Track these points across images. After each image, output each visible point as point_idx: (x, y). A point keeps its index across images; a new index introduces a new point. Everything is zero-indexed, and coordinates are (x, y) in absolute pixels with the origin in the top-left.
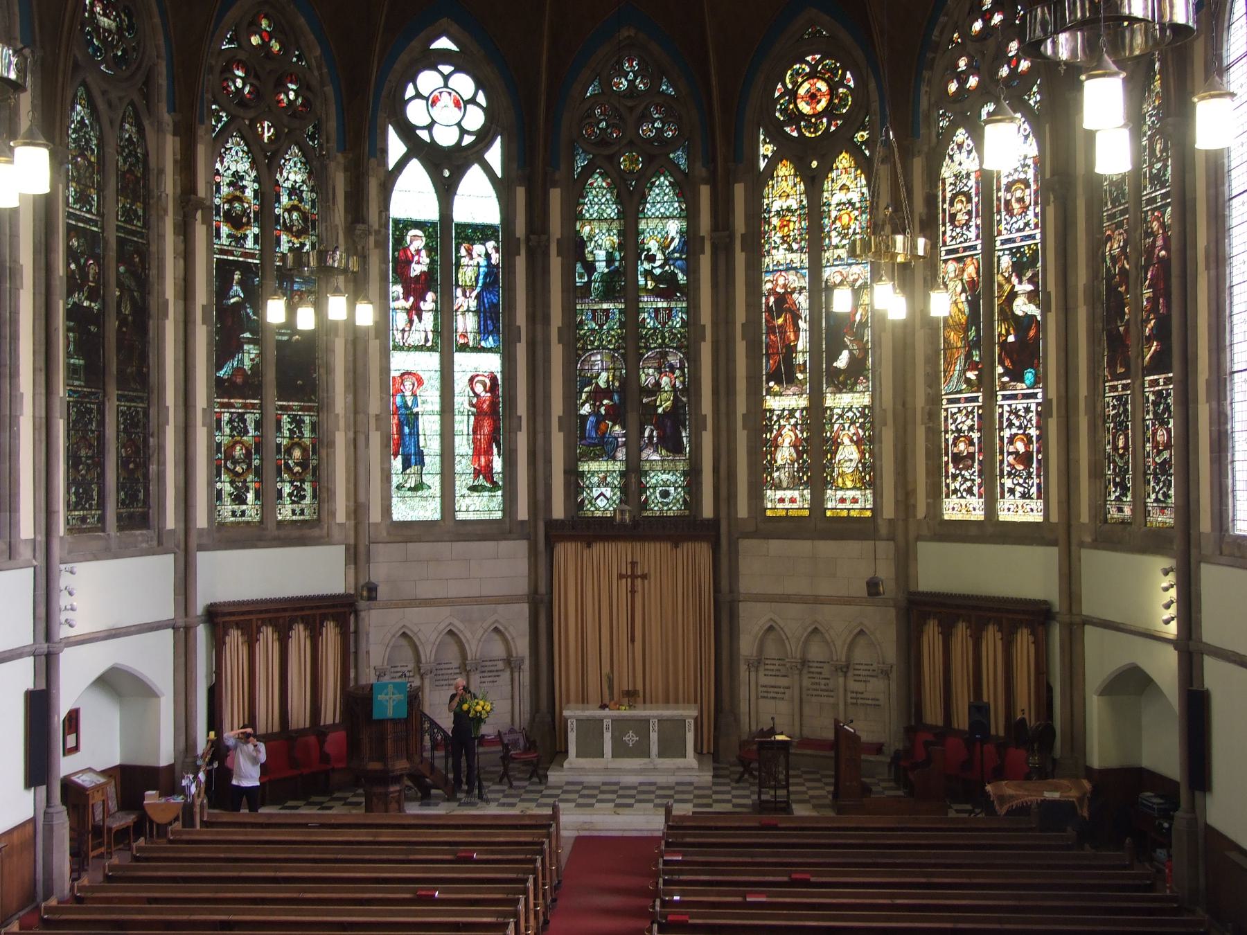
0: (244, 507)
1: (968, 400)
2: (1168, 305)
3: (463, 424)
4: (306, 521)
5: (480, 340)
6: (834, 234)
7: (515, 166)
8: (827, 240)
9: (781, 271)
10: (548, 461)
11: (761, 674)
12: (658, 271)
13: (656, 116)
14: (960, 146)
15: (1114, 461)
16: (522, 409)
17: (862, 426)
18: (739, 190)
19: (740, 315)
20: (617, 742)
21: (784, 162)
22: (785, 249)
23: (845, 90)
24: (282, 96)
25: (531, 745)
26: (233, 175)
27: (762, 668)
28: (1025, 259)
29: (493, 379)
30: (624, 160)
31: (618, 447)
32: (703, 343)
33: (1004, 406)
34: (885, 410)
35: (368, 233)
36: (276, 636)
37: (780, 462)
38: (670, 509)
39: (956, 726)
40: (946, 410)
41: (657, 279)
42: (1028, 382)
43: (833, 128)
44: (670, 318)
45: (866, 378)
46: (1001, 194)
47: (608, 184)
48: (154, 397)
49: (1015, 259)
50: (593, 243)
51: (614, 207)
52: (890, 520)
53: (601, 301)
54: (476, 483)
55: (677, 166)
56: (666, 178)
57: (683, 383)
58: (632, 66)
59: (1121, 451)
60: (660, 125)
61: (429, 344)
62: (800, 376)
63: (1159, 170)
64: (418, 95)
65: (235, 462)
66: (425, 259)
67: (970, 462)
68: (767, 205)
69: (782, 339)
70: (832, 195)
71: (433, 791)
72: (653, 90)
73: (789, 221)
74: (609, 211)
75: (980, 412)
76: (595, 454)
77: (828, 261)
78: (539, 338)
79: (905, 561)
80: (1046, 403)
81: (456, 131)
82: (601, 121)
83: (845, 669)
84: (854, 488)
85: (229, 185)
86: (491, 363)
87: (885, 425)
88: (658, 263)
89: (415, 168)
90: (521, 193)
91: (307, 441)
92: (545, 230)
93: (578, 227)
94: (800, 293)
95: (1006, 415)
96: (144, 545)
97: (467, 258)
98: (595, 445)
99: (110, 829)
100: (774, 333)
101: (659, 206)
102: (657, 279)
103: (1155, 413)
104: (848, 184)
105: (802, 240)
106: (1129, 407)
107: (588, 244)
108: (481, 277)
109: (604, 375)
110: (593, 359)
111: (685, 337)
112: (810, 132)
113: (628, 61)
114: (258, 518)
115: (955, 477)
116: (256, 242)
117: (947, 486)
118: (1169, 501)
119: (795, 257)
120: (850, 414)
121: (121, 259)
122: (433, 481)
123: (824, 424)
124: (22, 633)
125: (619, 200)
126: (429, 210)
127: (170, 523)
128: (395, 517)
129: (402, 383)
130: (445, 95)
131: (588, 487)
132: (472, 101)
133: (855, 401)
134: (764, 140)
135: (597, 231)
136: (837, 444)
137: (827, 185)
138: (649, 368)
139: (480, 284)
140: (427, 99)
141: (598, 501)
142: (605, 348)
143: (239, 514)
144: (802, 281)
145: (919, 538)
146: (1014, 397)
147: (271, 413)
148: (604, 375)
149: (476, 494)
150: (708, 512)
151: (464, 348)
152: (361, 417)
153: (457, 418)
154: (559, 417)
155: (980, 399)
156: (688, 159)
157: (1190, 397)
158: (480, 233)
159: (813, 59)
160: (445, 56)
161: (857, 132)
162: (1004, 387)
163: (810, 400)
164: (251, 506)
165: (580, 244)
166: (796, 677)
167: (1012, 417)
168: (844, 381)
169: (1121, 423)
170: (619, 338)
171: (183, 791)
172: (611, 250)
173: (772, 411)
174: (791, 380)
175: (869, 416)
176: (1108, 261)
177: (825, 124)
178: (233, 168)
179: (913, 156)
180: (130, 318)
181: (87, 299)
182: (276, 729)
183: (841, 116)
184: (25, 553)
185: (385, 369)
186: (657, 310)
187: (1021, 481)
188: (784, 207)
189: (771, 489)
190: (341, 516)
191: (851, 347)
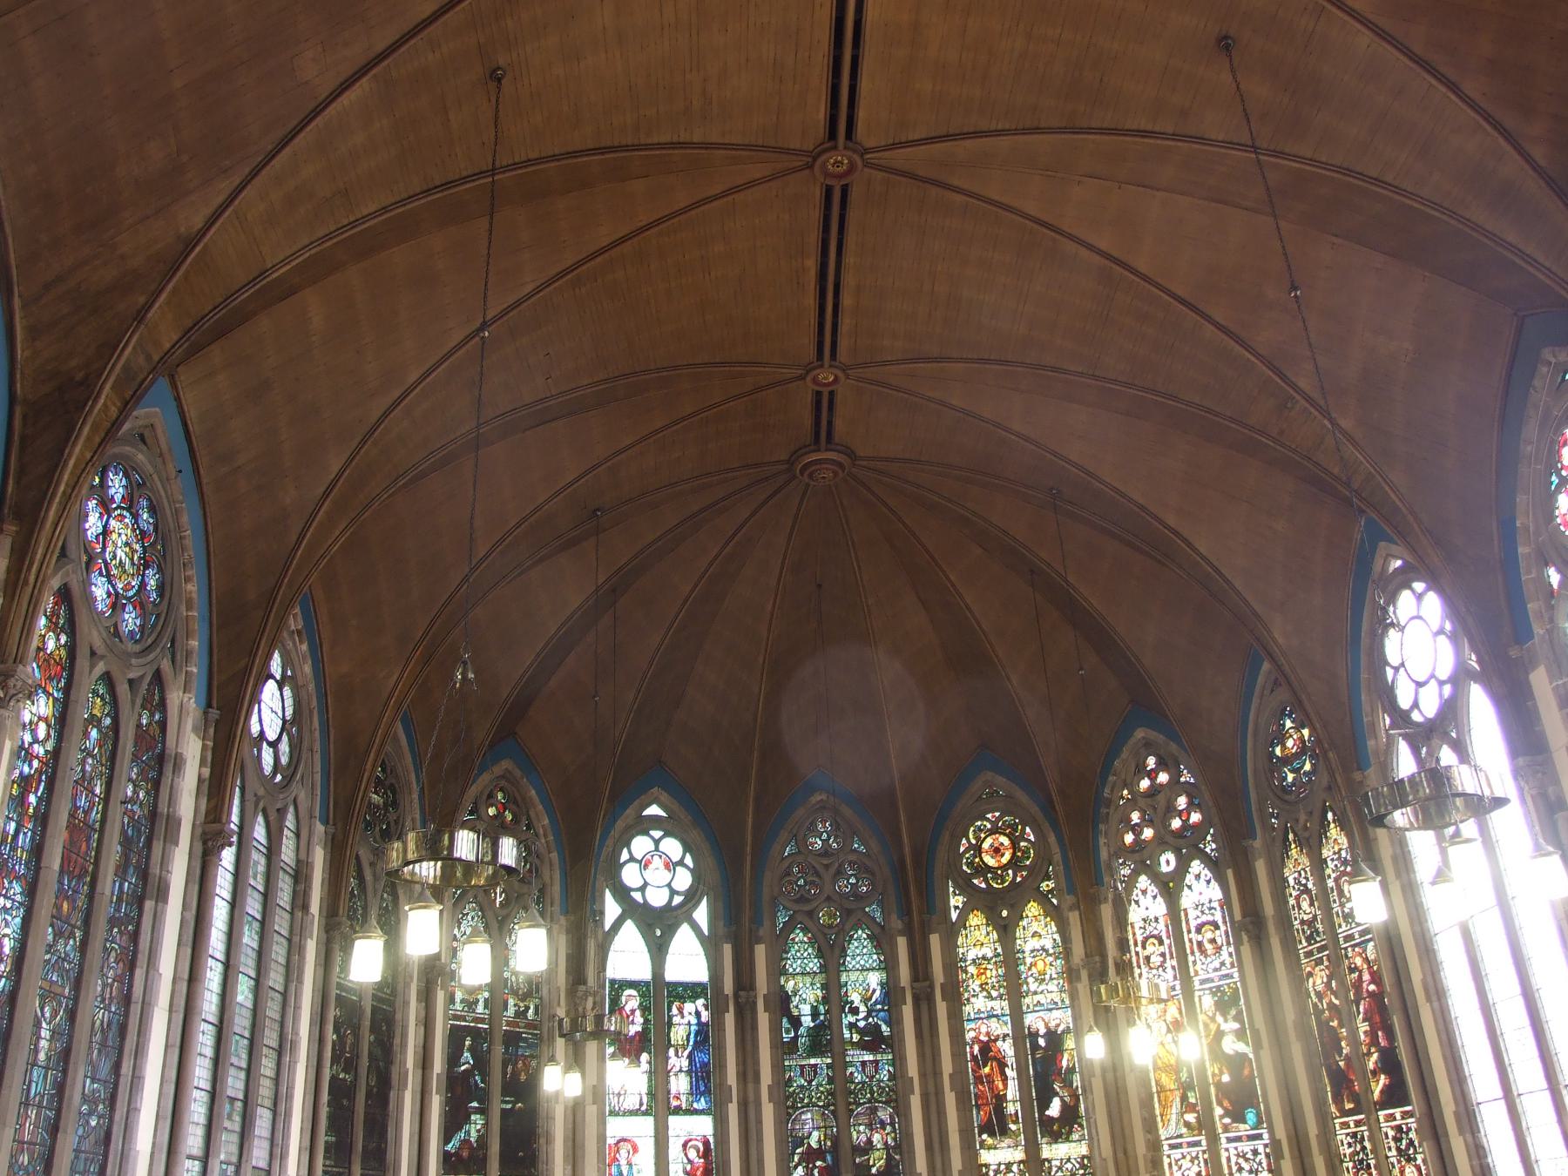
1: (1191, 1145)
5: (693, 1102)
6: (1030, 980)
7: (722, 923)
8: (1025, 986)
9: (982, 1019)
12: (862, 1024)
14: (1144, 892)
18: (935, 940)
19: (947, 1066)
21: (975, 912)
22: (985, 997)
23: (1026, 844)
28: (1226, 998)
29: (706, 1143)
30: (823, 915)
32: (912, 1096)
34: (1105, 1160)
35: (586, 994)
40: (1169, 1156)
41: (861, 1031)
42: (1250, 1122)
43: (1019, 879)
45: (1081, 1126)
47: (809, 938)
49: (1216, 998)
51: (816, 960)
53: (809, 1057)
55: (874, 919)
57: (895, 1139)
60: (854, 881)
61: (644, 1108)
62: (1013, 1127)
64: (632, 859)
66: (639, 1019)
68: (963, 954)
70: (1025, 942)
72: (846, 848)
73: (986, 969)
74: (811, 965)
75: (1206, 1156)
77: (1028, 1007)
78: (751, 1097)
80: (1275, 1144)
81: (666, 892)
82: (799, 879)
86: (703, 1126)
88: (862, 1015)
89: (630, 930)
90: (727, 949)
92: (751, 987)
94: (1004, 1040)
95: (1233, 1159)
97: (679, 1017)
100: (982, 1083)
101: (858, 958)
102: (861, 1031)
103: (1398, 1149)
104: (1039, 931)
105: (1000, 987)
106: (1367, 1144)
108: (692, 1036)
109: (815, 1134)
110: (803, 1117)
111: (893, 1090)
112: (997, 883)
116: (486, 1007)
119: (996, 1004)
120: (1069, 1166)
121: (373, 1030)
126: (643, 972)
129: (618, 1151)
130: (656, 858)
132: (681, 863)
134: (954, 892)
135: (801, 985)
138: (860, 1124)
140: (640, 862)
142: (815, 1105)
144: (1004, 1028)
146: (1239, 1139)
151: (678, 1111)
154: (1283, 1158)
155: (1204, 1143)
156: (882, 912)
157: (1440, 1131)
158: (691, 991)
159: (993, 817)
160: (655, 822)
161: (1042, 882)
163: (1026, 1152)
167: (1241, 1160)
168: (1059, 1130)
169: (1361, 1161)
170: (829, 1095)
173: (987, 1166)
174: (1004, 1131)
176: (1314, 997)
177: (1011, 875)
179: (1100, 903)
180: (375, 1090)
181: (342, 1071)
185: (602, 1137)
186: (864, 1063)
191: (1061, 1094)
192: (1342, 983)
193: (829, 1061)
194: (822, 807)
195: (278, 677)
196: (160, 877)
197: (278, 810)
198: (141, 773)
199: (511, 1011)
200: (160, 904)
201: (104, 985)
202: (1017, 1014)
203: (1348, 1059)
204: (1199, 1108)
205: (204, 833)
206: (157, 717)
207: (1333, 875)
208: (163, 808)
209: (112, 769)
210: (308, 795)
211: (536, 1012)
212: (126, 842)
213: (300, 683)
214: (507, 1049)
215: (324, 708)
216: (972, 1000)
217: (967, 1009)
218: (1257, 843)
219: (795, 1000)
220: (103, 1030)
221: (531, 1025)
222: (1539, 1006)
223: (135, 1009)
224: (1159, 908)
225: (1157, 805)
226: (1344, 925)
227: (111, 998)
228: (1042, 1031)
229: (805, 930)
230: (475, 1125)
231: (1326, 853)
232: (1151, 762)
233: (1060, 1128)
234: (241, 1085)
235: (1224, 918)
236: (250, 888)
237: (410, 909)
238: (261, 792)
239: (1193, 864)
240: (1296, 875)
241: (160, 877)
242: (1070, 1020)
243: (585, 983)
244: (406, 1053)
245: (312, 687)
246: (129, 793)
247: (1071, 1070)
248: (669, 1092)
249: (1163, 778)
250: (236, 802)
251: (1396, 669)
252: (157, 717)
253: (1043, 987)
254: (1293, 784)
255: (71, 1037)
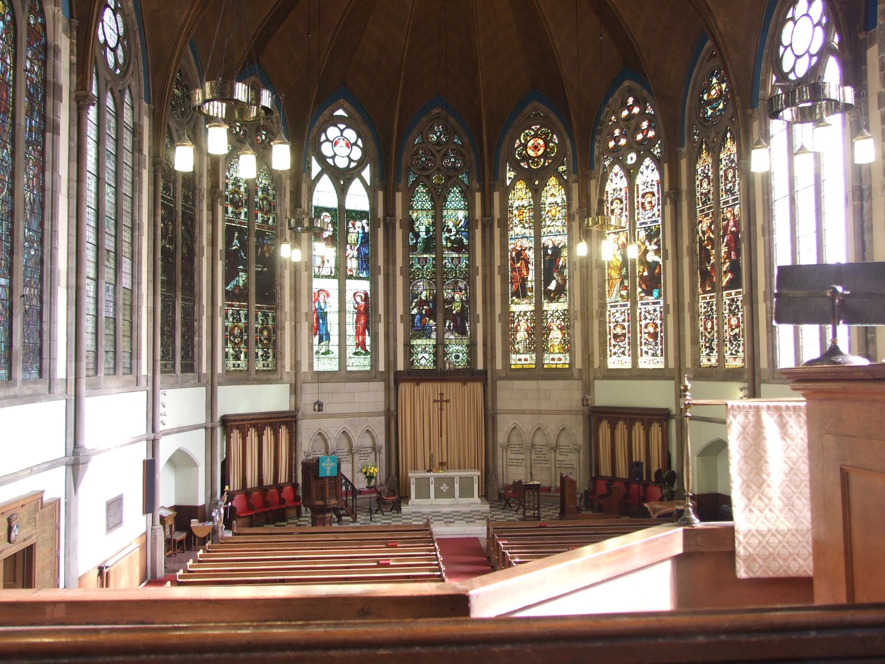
0: (239, 362)
2: (738, 253)
3: (351, 318)
4: (269, 371)
6: (547, 219)
7: (377, 179)
11: (509, 453)
12: (453, 238)
15: (705, 335)
16: (381, 311)
17: (563, 320)
18: (496, 195)
19: (497, 262)
20: (437, 490)
24: (259, 138)
25: (392, 492)
26: (235, 179)
27: (509, 450)
29: (366, 294)
33: (641, 309)
36: (256, 434)
37: (519, 339)
39: (618, 476)
40: (610, 311)
41: (451, 242)
43: (546, 164)
45: (566, 295)
46: (609, 205)
48: (197, 299)
53: (423, 253)
55: (463, 182)
56: (457, 188)
57: (466, 297)
58: (439, 128)
59: (709, 330)
61: (333, 275)
62: (530, 294)
63: (731, 187)
64: (327, 140)
65: (235, 337)
67: (623, 338)
69: (520, 275)
71: (343, 518)
74: (427, 205)
78: (391, 273)
79: (588, 388)
80: (666, 306)
81: (347, 160)
83: (555, 448)
84: (559, 353)
85: (233, 184)
86: (364, 286)
88: (453, 233)
89: (326, 180)
90: (381, 194)
91: (270, 326)
95: (643, 313)
96: (192, 382)
98: (419, 330)
99: (175, 540)
100: (515, 271)
102: (452, 242)
103: (730, 310)
106: (714, 308)
109: (424, 293)
114: (246, 368)
115: (615, 346)
116: (245, 216)
117: (611, 351)
118: (738, 354)
120: (557, 314)
122: (335, 349)
124: (141, 428)
125: (432, 199)
126: (333, 203)
127: (205, 369)
128: (316, 369)
132: (355, 144)
140: (332, 142)
143: (236, 366)
145: (595, 378)
146: (648, 304)
147: (253, 310)
148: (424, 293)
150: (480, 366)
151: (351, 277)
152: (298, 314)
153: (348, 315)
155: (629, 305)
158: (360, 215)
160: (341, 119)
162: (641, 298)
164: (242, 362)
165: (412, 222)
166: (528, 454)
167: (647, 314)
168: (553, 296)
169: (709, 316)
171: (212, 519)
173: (514, 313)
174: (525, 296)
175: (566, 315)
178: (235, 176)
179: (591, 179)
182: (256, 485)
183: (551, 158)
184: (143, 382)
185: (310, 288)
186: (452, 258)
187: (652, 347)
190: (288, 368)
192: (717, 226)
193: (434, 256)
194: (438, 117)
195: (113, 7)
196: (53, 120)
197: (120, 91)
198: (34, 54)
199: (260, 220)
200: (55, 136)
201: (28, 179)
202: (538, 237)
203: (713, 265)
204: (629, 288)
205: (77, 96)
206: (40, 20)
207: (724, 168)
208: (50, 77)
209: (15, 48)
210: (136, 82)
211: (274, 221)
212: (30, 97)
213: (127, 13)
214: (258, 240)
215: (143, 31)
216: (514, 228)
217: (511, 233)
218: (684, 150)
219: (417, 224)
220: (31, 203)
221: (270, 228)
222: (824, 237)
223: (48, 194)
224: (623, 183)
225: (630, 126)
226: (724, 195)
227: (33, 186)
228: (551, 246)
229: (424, 186)
230: (241, 279)
231: (722, 156)
232: (631, 101)
233: (555, 295)
234: (112, 244)
235: (658, 190)
236: (107, 136)
237: (210, 127)
238: (109, 78)
239: (646, 160)
240: (703, 168)
241: (53, 120)
242: (566, 241)
243: (301, 207)
244: (202, 237)
245: (134, 16)
246: (28, 67)
247: (564, 267)
248: (346, 268)
249: (636, 110)
250: (94, 82)
251: (786, 48)
252: (40, 20)
253: (554, 223)
254: (711, 116)
255: (13, 205)
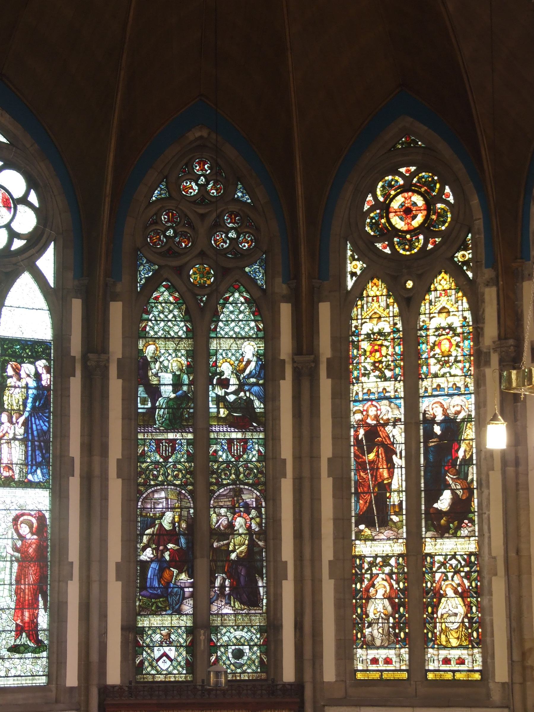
5: (27, 473)
6: (432, 361)
7: (70, 275)
9: (372, 400)
10: (103, 616)
12: (231, 398)
13: (231, 225)
17: (468, 576)
21: (375, 280)
22: (378, 377)
29: (41, 518)
30: (194, 273)
31: (184, 598)
34: (495, 558)
37: (372, 616)
38: (244, 672)
41: (229, 406)
43: (430, 246)
44: (245, 451)
45: (472, 521)
47: (175, 298)
50: (158, 364)
51: (182, 324)
52: (503, 684)
53: (167, 431)
54: (18, 642)
55: (254, 281)
56: (240, 293)
57: (259, 525)
58: (203, 169)
62: (395, 518)
68: (356, 327)
70: (431, 318)
73: (381, 345)
74: (176, 329)
76: (158, 607)
77: (426, 390)
78: (97, 471)
82: (168, 229)
87: (496, 574)
88: (232, 389)
90: (77, 305)
93: (141, 346)
94: (394, 426)
97: (14, 379)
98: (157, 596)
100: (365, 470)
101: (233, 324)
102: (229, 406)
105: (396, 366)
107: (152, 365)
108: (30, 400)
109: (169, 515)
112: (404, 249)
113: (199, 163)
119: (390, 386)
120: (454, 562)
123: (424, 573)
125: (188, 317)
131: (148, 646)
132: (24, 200)
133: (459, 547)
134: (353, 256)
136: (439, 596)
137: (424, 308)
138: (221, 507)
139: (28, 409)
141: (160, 663)
144: (396, 412)
148: (169, 515)
149: (17, 656)
156: (266, 273)
159: (407, 171)
161: (458, 251)
163: (407, 545)
170: (187, 473)
172: (178, 373)
173: (362, 558)
174: (385, 523)
177: (422, 241)
186: (230, 441)
188: (376, 330)
189: (362, 648)
191: (453, 486)
